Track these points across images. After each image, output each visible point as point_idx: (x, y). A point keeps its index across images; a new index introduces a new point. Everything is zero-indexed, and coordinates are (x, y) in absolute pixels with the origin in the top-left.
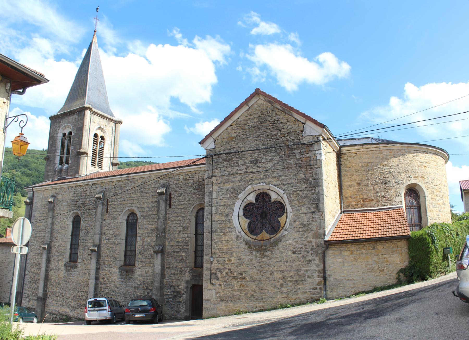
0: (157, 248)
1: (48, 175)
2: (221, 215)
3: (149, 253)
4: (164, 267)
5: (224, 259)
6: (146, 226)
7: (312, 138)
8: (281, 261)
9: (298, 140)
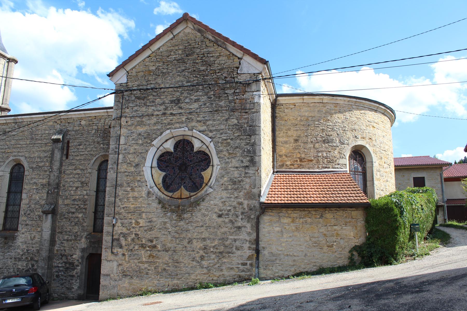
0: (47, 208)
2: (129, 165)
3: (36, 213)
4: (55, 231)
5: (130, 221)
6: (35, 180)
7: (249, 76)
8: (202, 226)
9: (231, 77)
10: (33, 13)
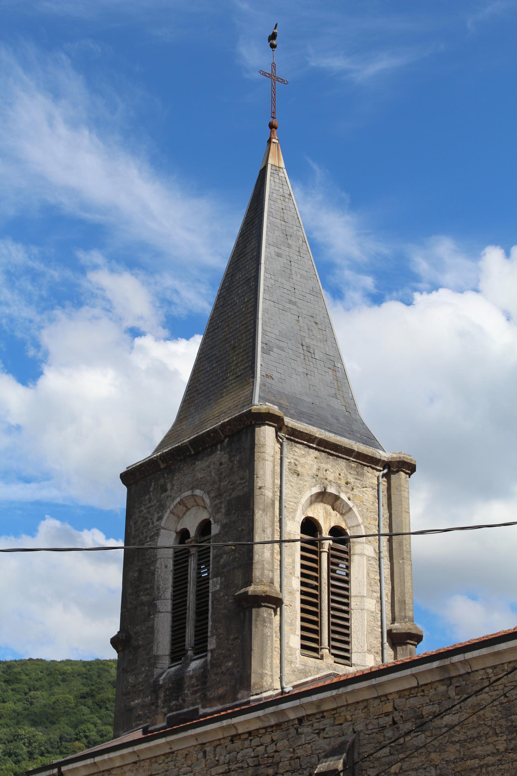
1: (130, 710)
10: (435, 287)
